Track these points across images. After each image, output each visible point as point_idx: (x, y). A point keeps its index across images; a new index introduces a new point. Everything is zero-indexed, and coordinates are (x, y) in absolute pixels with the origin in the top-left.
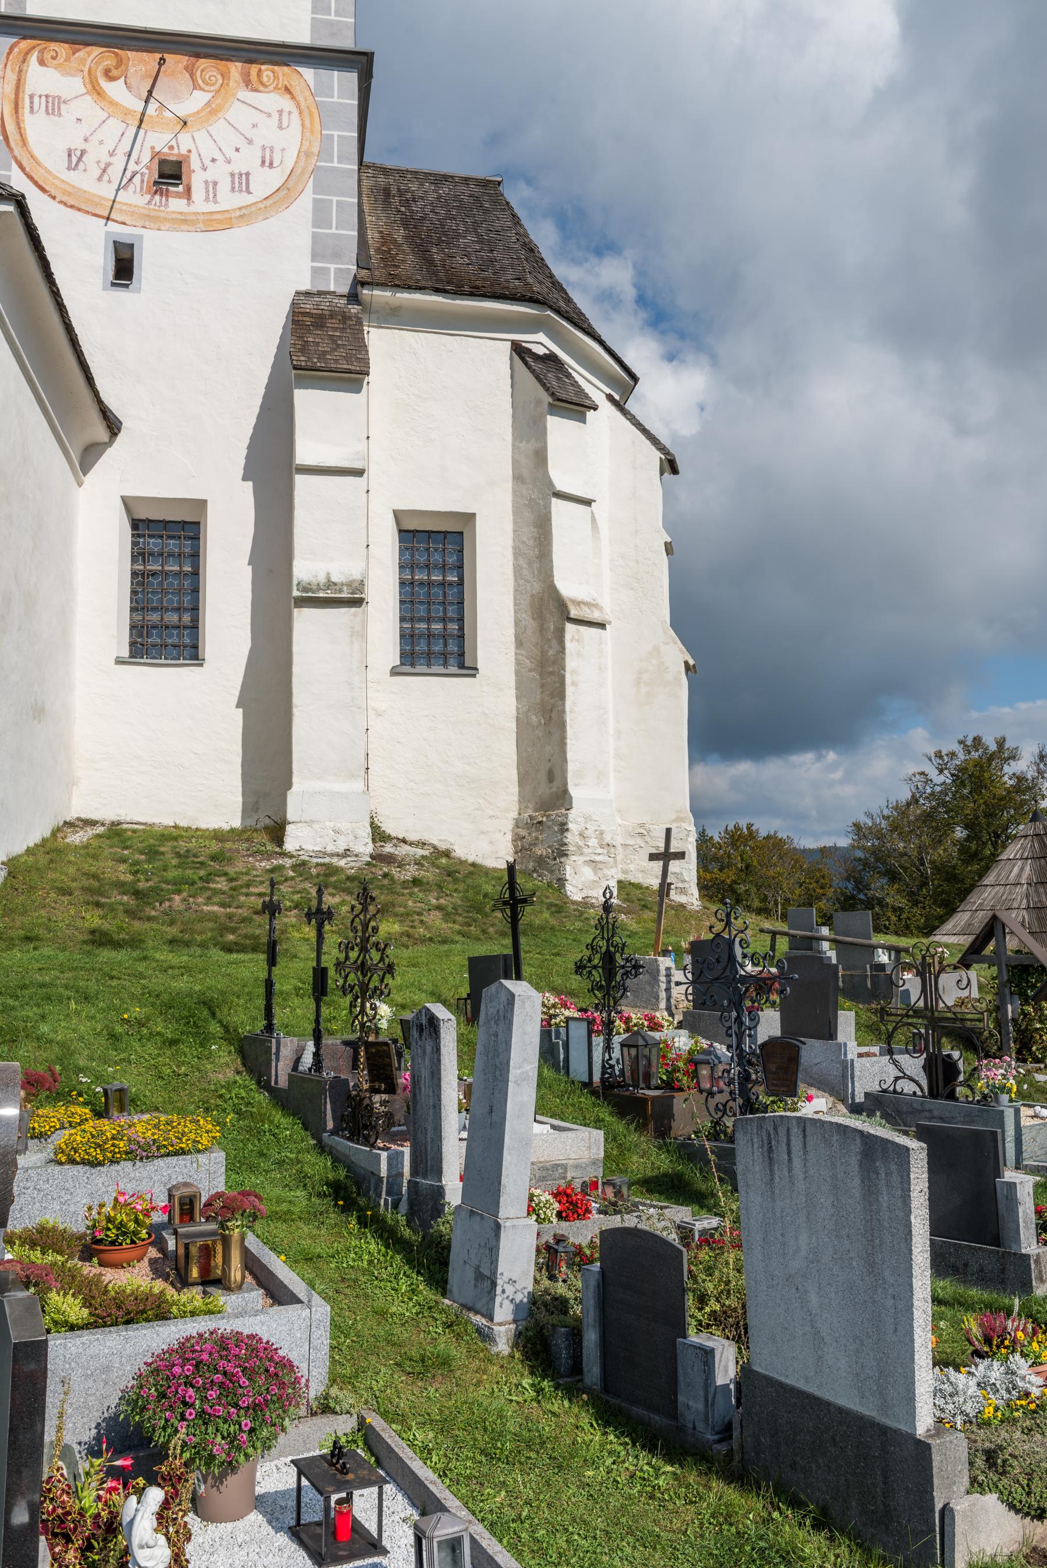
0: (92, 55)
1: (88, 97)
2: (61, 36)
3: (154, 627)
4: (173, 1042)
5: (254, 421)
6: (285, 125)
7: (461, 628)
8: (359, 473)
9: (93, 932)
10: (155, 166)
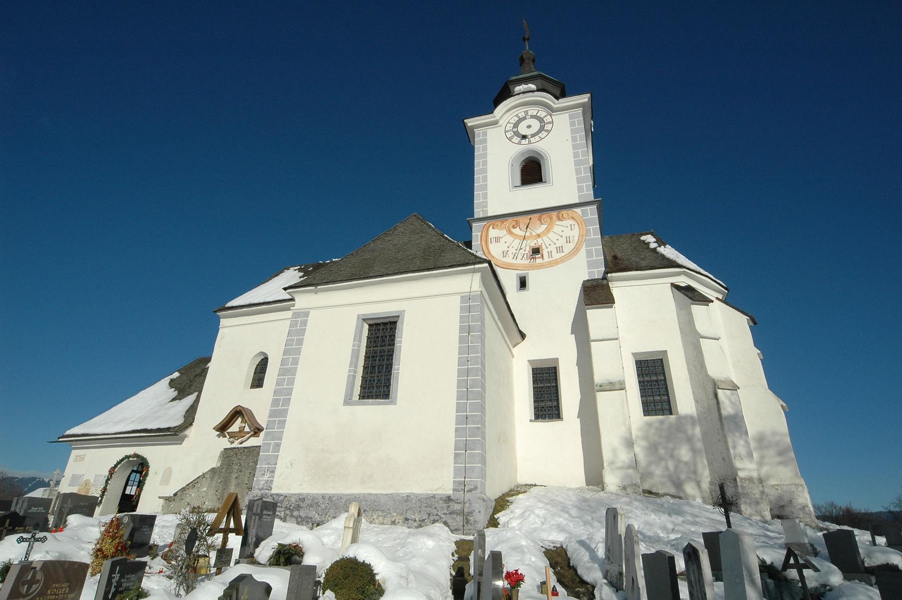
0: (510, 221)
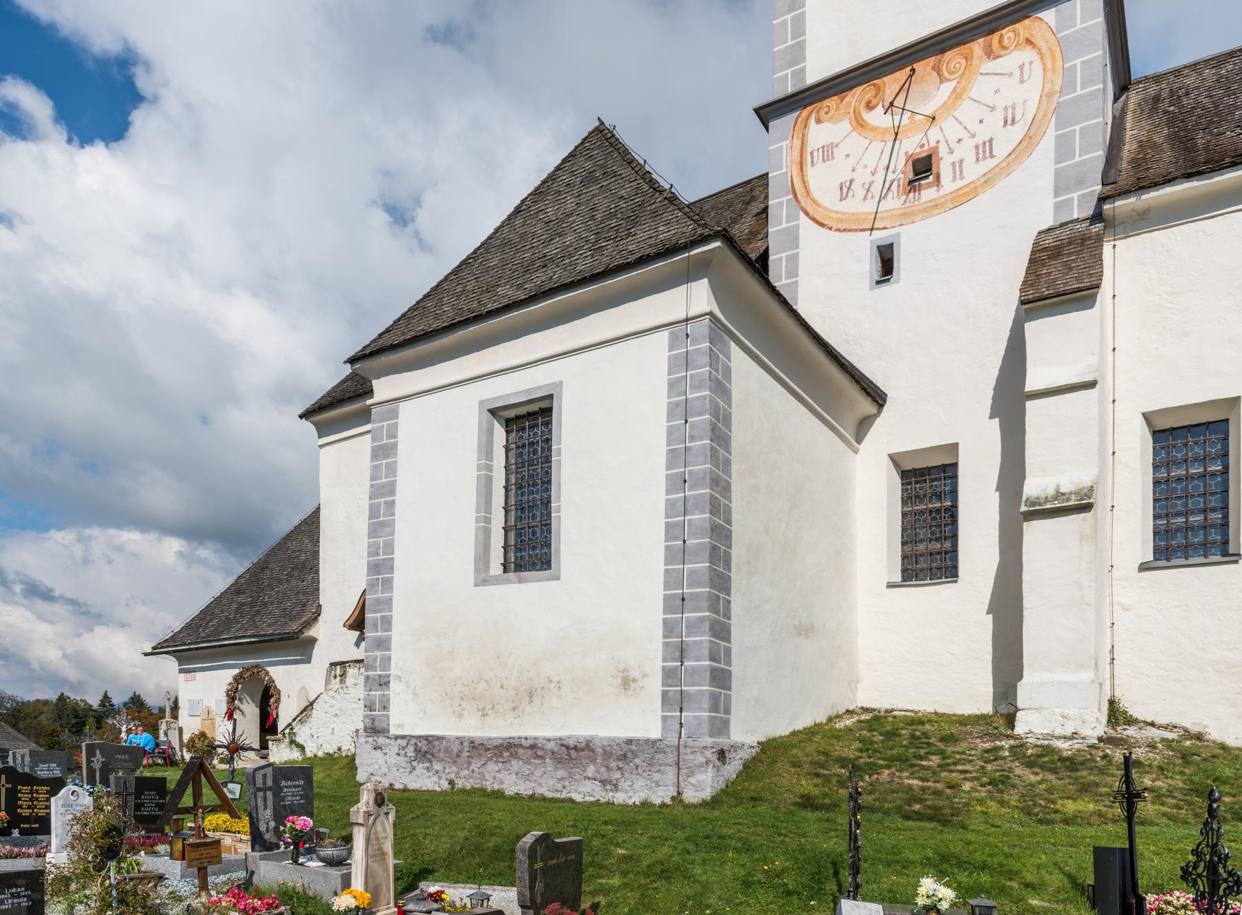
1: (854, 133)
2: (831, 92)
3: (921, 555)
4: (789, 893)
5: (999, 363)
6: (1026, 76)
7: (1226, 516)
8: (1091, 385)
9: (802, 796)
10: (910, 168)
